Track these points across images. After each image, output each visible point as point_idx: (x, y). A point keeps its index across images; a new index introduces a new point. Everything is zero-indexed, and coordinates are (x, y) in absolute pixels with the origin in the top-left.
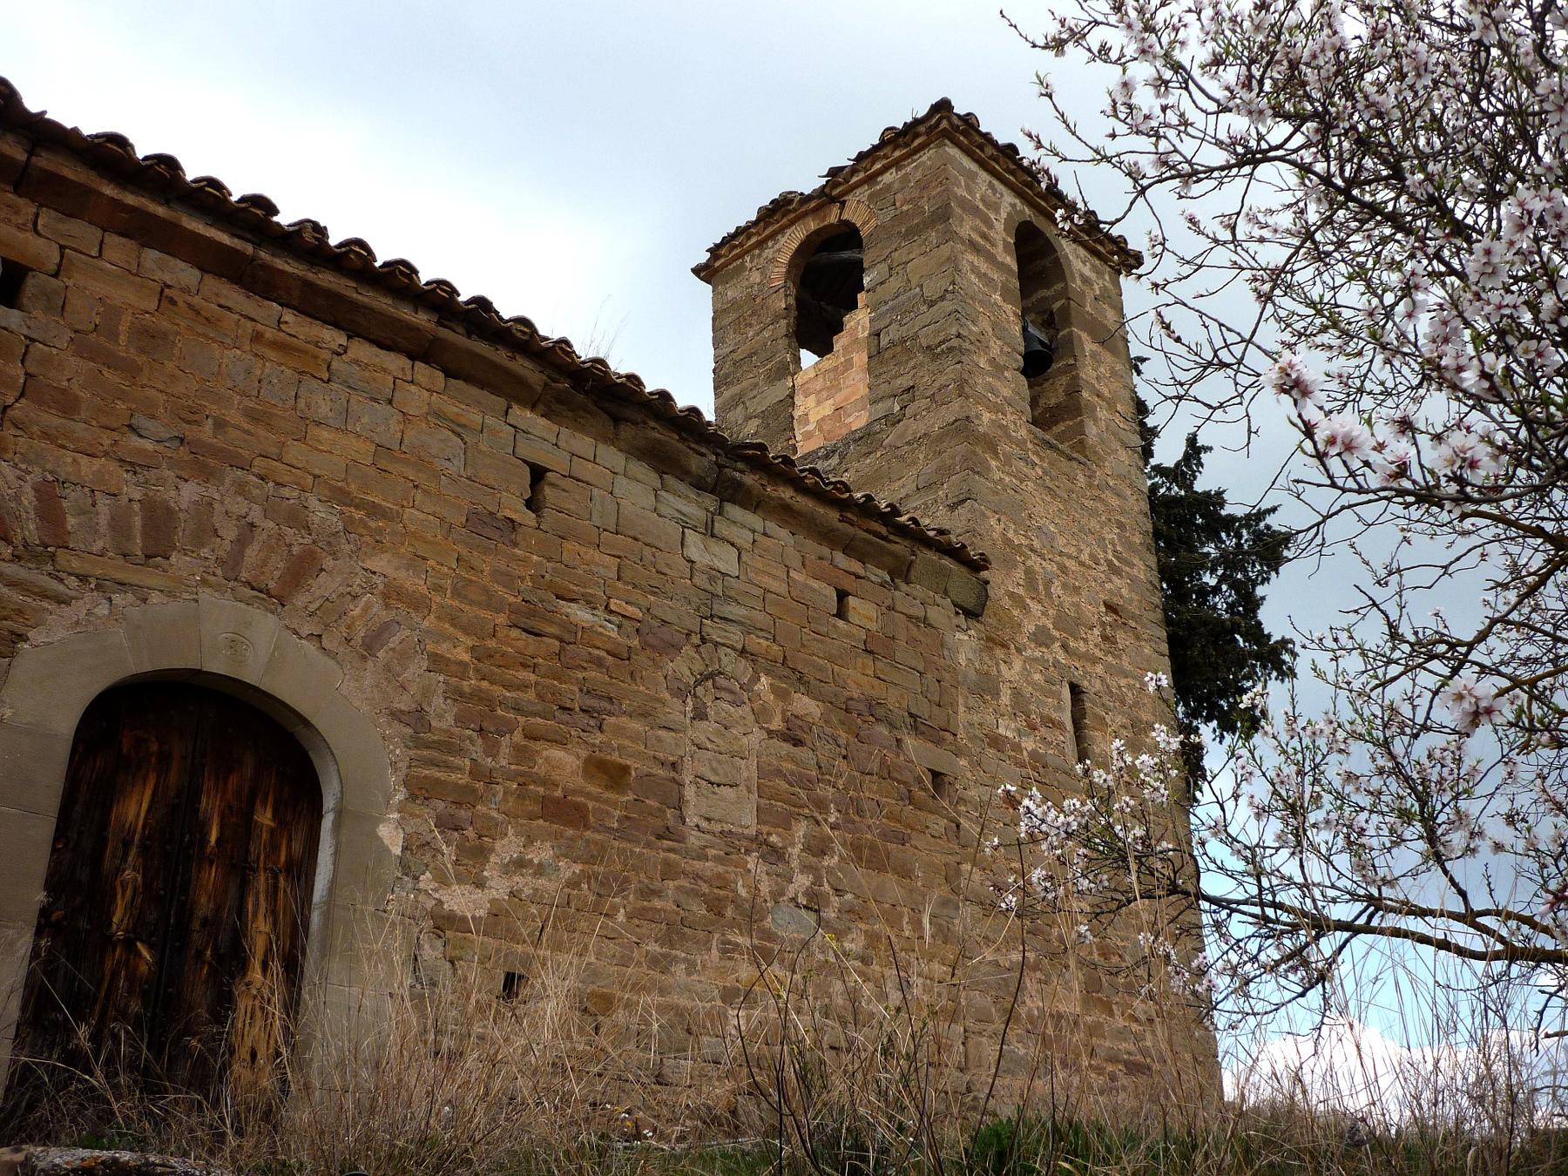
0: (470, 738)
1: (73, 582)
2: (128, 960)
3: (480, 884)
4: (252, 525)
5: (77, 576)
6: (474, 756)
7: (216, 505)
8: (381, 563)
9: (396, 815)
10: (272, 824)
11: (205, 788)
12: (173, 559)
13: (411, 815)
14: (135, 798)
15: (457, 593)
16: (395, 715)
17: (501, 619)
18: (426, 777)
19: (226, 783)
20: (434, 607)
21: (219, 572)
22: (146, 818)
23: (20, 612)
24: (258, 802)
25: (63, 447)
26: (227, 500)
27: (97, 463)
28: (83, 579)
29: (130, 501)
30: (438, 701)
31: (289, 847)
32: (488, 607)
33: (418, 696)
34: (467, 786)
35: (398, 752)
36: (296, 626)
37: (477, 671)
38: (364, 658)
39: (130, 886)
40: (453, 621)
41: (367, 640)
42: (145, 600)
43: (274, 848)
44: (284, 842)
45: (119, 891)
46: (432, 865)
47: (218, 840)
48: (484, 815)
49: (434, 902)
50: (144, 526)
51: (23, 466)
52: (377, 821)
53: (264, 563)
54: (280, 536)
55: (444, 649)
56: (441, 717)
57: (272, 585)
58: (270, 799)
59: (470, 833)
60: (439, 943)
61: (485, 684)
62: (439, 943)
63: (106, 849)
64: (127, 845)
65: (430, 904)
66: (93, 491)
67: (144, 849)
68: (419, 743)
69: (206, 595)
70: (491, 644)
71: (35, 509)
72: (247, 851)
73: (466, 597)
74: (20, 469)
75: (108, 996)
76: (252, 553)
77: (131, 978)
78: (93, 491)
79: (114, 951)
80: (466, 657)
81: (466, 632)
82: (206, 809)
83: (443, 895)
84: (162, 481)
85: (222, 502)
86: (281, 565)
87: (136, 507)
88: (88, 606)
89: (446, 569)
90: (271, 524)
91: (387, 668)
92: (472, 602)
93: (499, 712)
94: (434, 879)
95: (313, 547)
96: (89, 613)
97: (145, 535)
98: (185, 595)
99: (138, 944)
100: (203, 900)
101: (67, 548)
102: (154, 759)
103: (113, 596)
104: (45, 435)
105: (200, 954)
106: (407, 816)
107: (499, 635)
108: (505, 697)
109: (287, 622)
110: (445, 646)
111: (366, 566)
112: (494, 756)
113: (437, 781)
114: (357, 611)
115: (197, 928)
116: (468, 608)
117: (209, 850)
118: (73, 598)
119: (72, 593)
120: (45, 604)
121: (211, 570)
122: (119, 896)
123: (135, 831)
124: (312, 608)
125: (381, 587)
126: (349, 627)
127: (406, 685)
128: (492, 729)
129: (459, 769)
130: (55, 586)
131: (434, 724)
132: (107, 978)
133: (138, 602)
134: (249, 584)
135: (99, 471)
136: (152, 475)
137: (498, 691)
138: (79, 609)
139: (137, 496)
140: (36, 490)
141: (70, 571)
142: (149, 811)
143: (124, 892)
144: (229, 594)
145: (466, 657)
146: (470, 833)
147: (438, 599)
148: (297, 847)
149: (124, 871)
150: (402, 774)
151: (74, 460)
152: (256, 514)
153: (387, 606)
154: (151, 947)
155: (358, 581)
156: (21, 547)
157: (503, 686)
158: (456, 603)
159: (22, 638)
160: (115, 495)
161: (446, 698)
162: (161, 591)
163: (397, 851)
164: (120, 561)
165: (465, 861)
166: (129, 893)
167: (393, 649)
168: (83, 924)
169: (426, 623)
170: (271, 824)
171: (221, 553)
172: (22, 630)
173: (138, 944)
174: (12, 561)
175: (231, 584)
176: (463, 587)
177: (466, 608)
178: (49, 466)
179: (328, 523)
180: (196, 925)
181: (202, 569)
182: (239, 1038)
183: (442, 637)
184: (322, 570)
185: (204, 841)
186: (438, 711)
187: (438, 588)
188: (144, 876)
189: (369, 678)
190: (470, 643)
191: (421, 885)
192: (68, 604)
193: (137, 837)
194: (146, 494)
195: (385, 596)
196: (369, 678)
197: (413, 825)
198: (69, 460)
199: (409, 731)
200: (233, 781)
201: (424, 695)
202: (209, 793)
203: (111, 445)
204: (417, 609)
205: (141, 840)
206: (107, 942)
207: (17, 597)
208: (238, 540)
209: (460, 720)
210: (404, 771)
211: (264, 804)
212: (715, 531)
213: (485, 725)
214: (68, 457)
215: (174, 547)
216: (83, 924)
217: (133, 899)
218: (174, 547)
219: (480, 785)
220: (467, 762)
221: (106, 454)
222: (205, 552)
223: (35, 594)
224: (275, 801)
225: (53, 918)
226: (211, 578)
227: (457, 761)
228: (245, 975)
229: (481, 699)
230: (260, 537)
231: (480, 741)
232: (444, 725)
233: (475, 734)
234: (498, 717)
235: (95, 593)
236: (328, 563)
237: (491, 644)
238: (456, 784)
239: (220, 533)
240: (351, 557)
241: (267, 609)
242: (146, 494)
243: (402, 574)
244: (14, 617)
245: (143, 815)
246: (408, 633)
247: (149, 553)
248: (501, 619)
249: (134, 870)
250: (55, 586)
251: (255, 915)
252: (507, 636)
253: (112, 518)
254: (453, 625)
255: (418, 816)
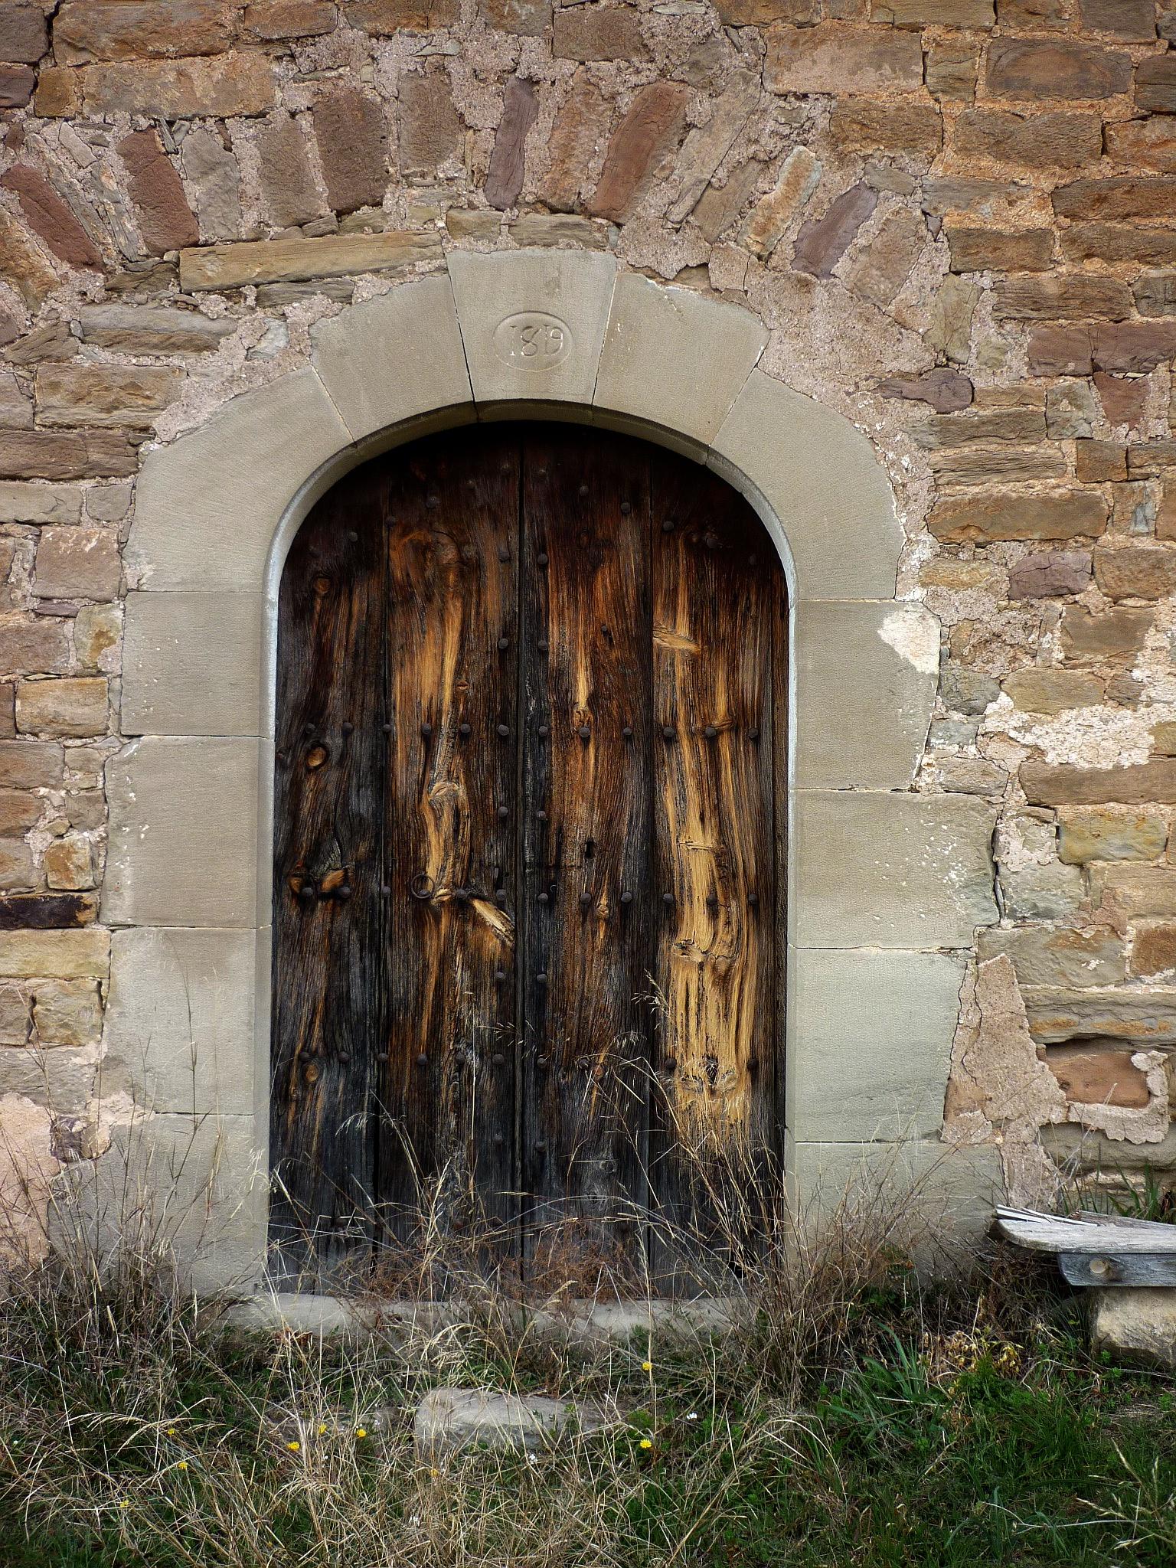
0: (1071, 395)
1: (215, 304)
2: (463, 934)
3: (1126, 696)
4: (531, 82)
5: (221, 291)
6: (1084, 430)
7: (453, 66)
8: (816, 71)
9: (919, 593)
10: (692, 647)
11: (552, 605)
12: (388, 202)
13: (950, 585)
14: (431, 651)
15: (1000, 82)
16: (889, 387)
17: (1119, 107)
18: (975, 501)
19: (591, 592)
20: (950, 129)
21: (480, 198)
22: (455, 685)
23: (133, 388)
24: (660, 600)
25: (159, 55)
26: (472, 47)
27: (219, 63)
28: (232, 292)
29: (293, 115)
30: (985, 333)
31: (731, 683)
32: (1082, 89)
33: (937, 336)
34: (1071, 499)
35: (906, 461)
36: (650, 261)
37: (1071, 241)
38: (805, 285)
39: (446, 808)
40: (1000, 145)
41: (804, 246)
42: (348, 299)
43: (702, 691)
44: (721, 676)
45: (429, 818)
46: (1011, 679)
47: (593, 699)
48: (1125, 553)
49: (1024, 753)
50: (325, 154)
51: (97, 118)
52: (875, 615)
53: (567, 151)
54: (590, 85)
55: (987, 215)
56: (995, 365)
57: (589, 190)
58: (682, 600)
59: (1092, 596)
60: (1045, 833)
61: (1094, 267)
62: (1045, 833)
63: (394, 752)
64: (429, 739)
65: (1014, 758)
66: (222, 120)
67: (462, 739)
68: (948, 432)
69: (461, 252)
70: (1101, 170)
71: (131, 189)
72: (650, 703)
73: (1025, 84)
74: (95, 126)
75: (438, 1008)
76: (537, 141)
77: (473, 965)
78: (222, 120)
79: (438, 922)
80: (1040, 218)
81: (1032, 160)
82: (561, 646)
83: (1044, 735)
84: (343, 56)
85: (462, 56)
86: (602, 144)
87: (305, 122)
88: (246, 343)
89: (969, 36)
90: (569, 66)
91: (859, 291)
92: (1040, 92)
93: (1137, 318)
94: (1020, 706)
95: (664, 84)
96: (250, 353)
97: (332, 172)
98: (422, 266)
99: (477, 904)
100: (581, 810)
101: (196, 245)
102: (452, 577)
103: (287, 309)
104: (126, 45)
105: (587, 907)
106: (943, 590)
107: (1116, 145)
108: (1148, 282)
109: (632, 257)
110: (987, 207)
111: (781, 88)
112: (1133, 421)
113: (1002, 503)
114: (779, 188)
115: (577, 861)
116: (1033, 106)
117: (576, 718)
118: (220, 335)
119: (215, 326)
120: (175, 361)
121: (463, 201)
122: (431, 830)
123: (439, 712)
124: (678, 212)
125: (822, 122)
126: (762, 230)
127: (907, 316)
128: (1120, 362)
129: (1049, 466)
130: (189, 321)
131: (979, 384)
132: (434, 968)
133: (337, 306)
134: (544, 203)
135: (226, 78)
136: (322, 49)
137: (1129, 272)
138: (229, 357)
139: (302, 101)
140: (126, 155)
141: (207, 285)
142: (458, 671)
143: (438, 819)
144: (505, 238)
145: (1040, 218)
146: (1092, 596)
147: (958, 109)
148: (749, 678)
149: (432, 782)
150: (920, 508)
151: (181, 73)
152: (534, 56)
153: (843, 159)
154: (500, 906)
155: (771, 125)
156: (120, 270)
157: (1141, 258)
158: (1002, 105)
159: (146, 431)
160: (262, 115)
161: (1001, 322)
162: (376, 271)
163: (928, 664)
164: (296, 236)
165: (1087, 657)
166: (447, 819)
167: (865, 249)
168: (377, 885)
169: (937, 169)
170: (692, 647)
171: (478, 160)
172: (138, 417)
173: (477, 904)
174: (109, 299)
175: (505, 216)
176: (1015, 63)
177: (1029, 108)
178: (139, 102)
179: (687, 21)
180: (573, 856)
181: (445, 204)
182: (680, 1043)
183: (981, 188)
184: (689, 126)
185: (565, 707)
186: (987, 353)
187: (955, 85)
188: (469, 788)
189: (822, 327)
190: (1047, 185)
191: (990, 725)
192: (210, 347)
193: (445, 721)
194: (319, 92)
195: (835, 140)
196: (822, 327)
197: (959, 606)
198: (171, 77)
199: (926, 412)
200: (603, 584)
201: (951, 329)
202: (561, 614)
203: (240, 19)
204: (911, 145)
205: (454, 723)
206: (422, 911)
207: (126, 361)
208: (509, 123)
209: (1043, 360)
210: (925, 498)
211: (672, 608)
212: (252, 236)
213: (1101, 356)
214: (168, 70)
215: (386, 178)
216: (377, 885)
217: (456, 831)
218: (386, 178)
219: (1104, 491)
220: (1069, 447)
221: (235, 39)
222: (447, 167)
223: (156, 347)
224: (691, 601)
225: (327, 885)
226: (470, 216)
227: (1045, 450)
228: (674, 931)
229: (1086, 302)
230: (550, 100)
231: (1095, 394)
232: (1003, 381)
233: (1081, 382)
234: (1134, 332)
235: (260, 313)
236: (700, 107)
237: (1101, 170)
238: (1047, 502)
239: (469, 120)
240: (747, 80)
241: (586, 244)
242: (319, 92)
243: (869, 78)
244: (127, 400)
245: (448, 679)
246: (897, 202)
247: (342, 204)
248: (1119, 107)
249: (449, 779)
250: (189, 321)
251: (682, 820)
252: (1137, 142)
253: (266, 160)
254: (1004, 157)
255: (969, 586)
